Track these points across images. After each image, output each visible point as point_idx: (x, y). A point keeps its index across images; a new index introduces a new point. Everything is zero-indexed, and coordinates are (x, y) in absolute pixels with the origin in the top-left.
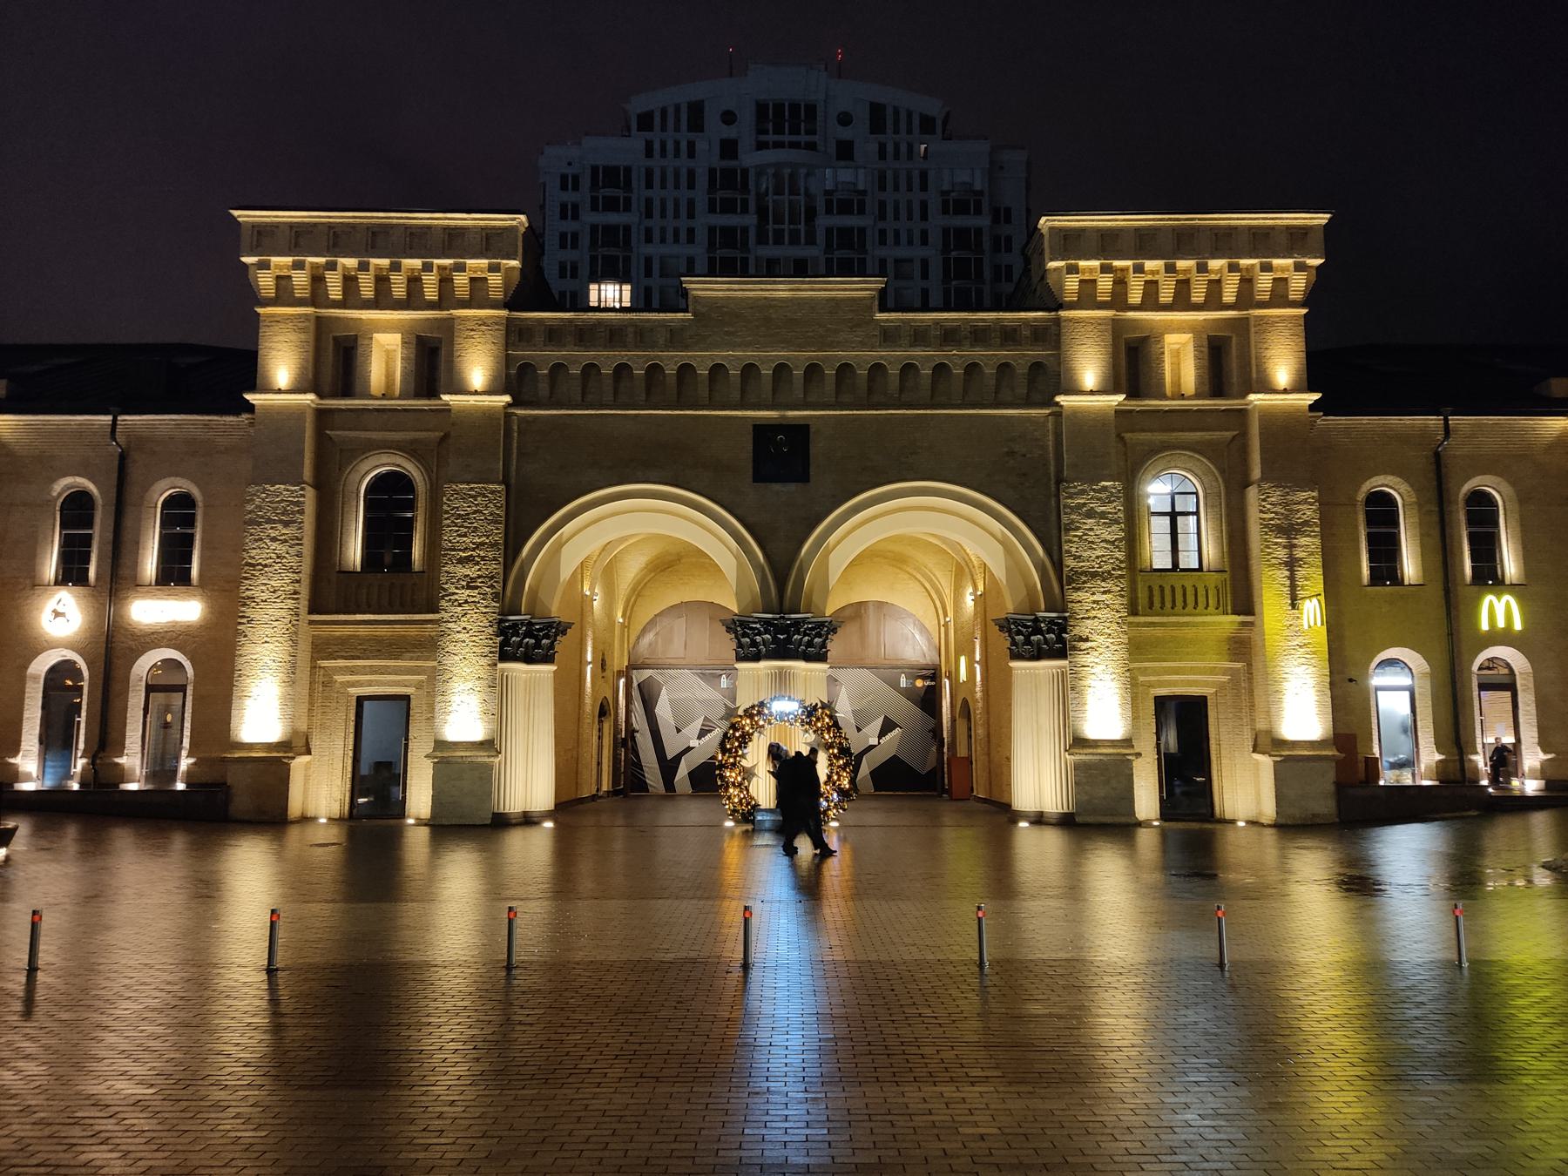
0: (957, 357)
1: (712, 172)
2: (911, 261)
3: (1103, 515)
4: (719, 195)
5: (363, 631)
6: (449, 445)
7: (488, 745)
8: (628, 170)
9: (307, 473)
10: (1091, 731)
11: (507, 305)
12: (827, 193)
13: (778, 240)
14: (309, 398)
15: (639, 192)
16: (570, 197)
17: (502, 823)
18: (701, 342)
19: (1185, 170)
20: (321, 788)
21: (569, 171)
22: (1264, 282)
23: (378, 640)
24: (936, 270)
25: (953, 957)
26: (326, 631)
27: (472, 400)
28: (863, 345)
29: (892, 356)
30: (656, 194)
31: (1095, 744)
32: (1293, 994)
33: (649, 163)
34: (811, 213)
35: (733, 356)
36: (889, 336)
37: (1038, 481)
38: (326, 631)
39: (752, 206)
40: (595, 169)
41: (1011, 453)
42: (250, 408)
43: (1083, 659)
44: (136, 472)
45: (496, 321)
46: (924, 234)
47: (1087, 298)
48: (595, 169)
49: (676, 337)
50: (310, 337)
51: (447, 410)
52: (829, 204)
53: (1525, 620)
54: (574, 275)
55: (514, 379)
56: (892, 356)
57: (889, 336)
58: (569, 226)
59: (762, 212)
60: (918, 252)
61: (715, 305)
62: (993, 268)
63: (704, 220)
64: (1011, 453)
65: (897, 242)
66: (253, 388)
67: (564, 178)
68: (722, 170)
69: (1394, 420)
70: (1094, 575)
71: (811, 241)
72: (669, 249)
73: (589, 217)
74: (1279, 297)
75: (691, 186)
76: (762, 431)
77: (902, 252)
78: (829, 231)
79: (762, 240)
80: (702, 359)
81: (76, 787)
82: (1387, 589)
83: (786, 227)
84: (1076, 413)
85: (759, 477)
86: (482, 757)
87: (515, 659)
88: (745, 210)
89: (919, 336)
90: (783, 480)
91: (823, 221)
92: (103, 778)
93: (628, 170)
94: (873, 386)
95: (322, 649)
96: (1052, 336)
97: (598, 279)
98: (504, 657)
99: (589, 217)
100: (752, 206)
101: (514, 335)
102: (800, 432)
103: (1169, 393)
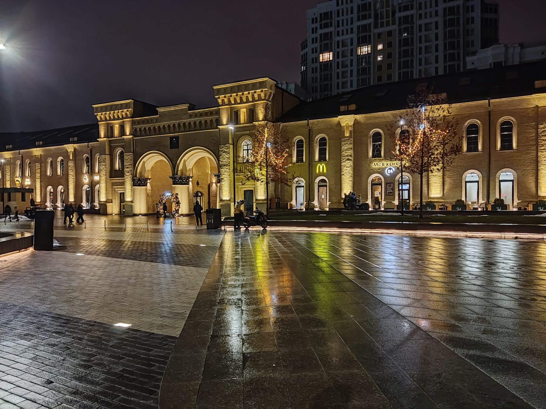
0: (203, 119)
1: (359, 6)
2: (431, 23)
3: (226, 152)
4: (361, 14)
5: (118, 181)
6: (125, 145)
7: (132, 202)
8: (331, 12)
9: (107, 152)
10: (224, 198)
11: (132, 118)
12: (399, 4)
13: (382, 26)
14: (105, 139)
15: (335, 19)
16: (314, 26)
17: (135, 215)
18: (161, 121)
19: (240, 73)
20: (114, 208)
21: (314, 17)
22: (256, 96)
23: (120, 182)
24: (441, 26)
25: (185, 243)
26: (113, 181)
27: (127, 137)
28: (186, 118)
29: (192, 120)
30: (340, 18)
31: (224, 201)
32: (539, 288)
33: (338, 8)
34: (394, 13)
35: (166, 123)
36: (191, 116)
37: (215, 146)
38: (113, 181)
39: (372, 16)
40: (321, 14)
41: (212, 139)
42: (98, 141)
43: (223, 183)
44: (93, 153)
45: (130, 121)
46: (436, 12)
47: (224, 104)
48: (321, 14)
49: (157, 121)
50: (106, 127)
51: (124, 139)
52: (400, 8)
53: (327, 170)
54: (316, 52)
55: (134, 133)
56: (192, 120)
57: (191, 116)
58: (314, 36)
59: (376, 17)
60: (435, 19)
61: (163, 113)
62: (204, 101)
63: (356, 24)
64: (212, 139)
65: (426, 17)
66: (99, 138)
67: (313, 19)
68: (362, 5)
69: (299, 122)
70: (225, 165)
71: (394, 23)
72: (345, 37)
73: (320, 31)
74: (260, 99)
75: (352, 13)
76: (172, 138)
77: (428, 21)
78: (400, 18)
79: (376, 27)
80: (161, 124)
81: (327, 209)
82: (300, 163)
83: (385, 20)
84: (222, 129)
85: (171, 148)
86: (130, 204)
87: (136, 186)
88: (370, 17)
89: (196, 115)
90: (174, 149)
91: (398, 15)
92: (92, 207)
93: (331, 12)
94: (187, 127)
95: (113, 184)
96: (218, 113)
97: (322, 52)
98: (134, 186)
99: (320, 31)
100: (372, 16)
101: (133, 123)
102: (177, 138)
103: (242, 122)
